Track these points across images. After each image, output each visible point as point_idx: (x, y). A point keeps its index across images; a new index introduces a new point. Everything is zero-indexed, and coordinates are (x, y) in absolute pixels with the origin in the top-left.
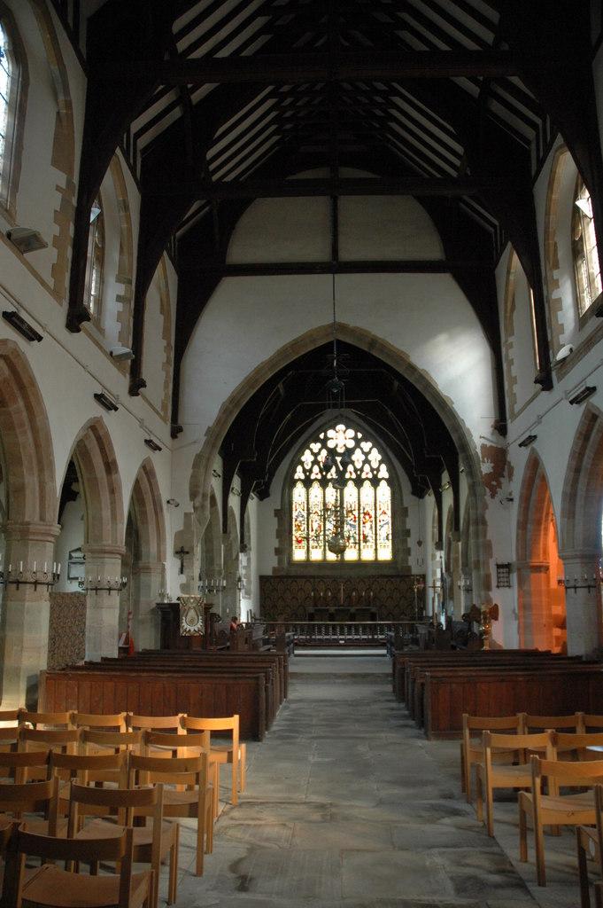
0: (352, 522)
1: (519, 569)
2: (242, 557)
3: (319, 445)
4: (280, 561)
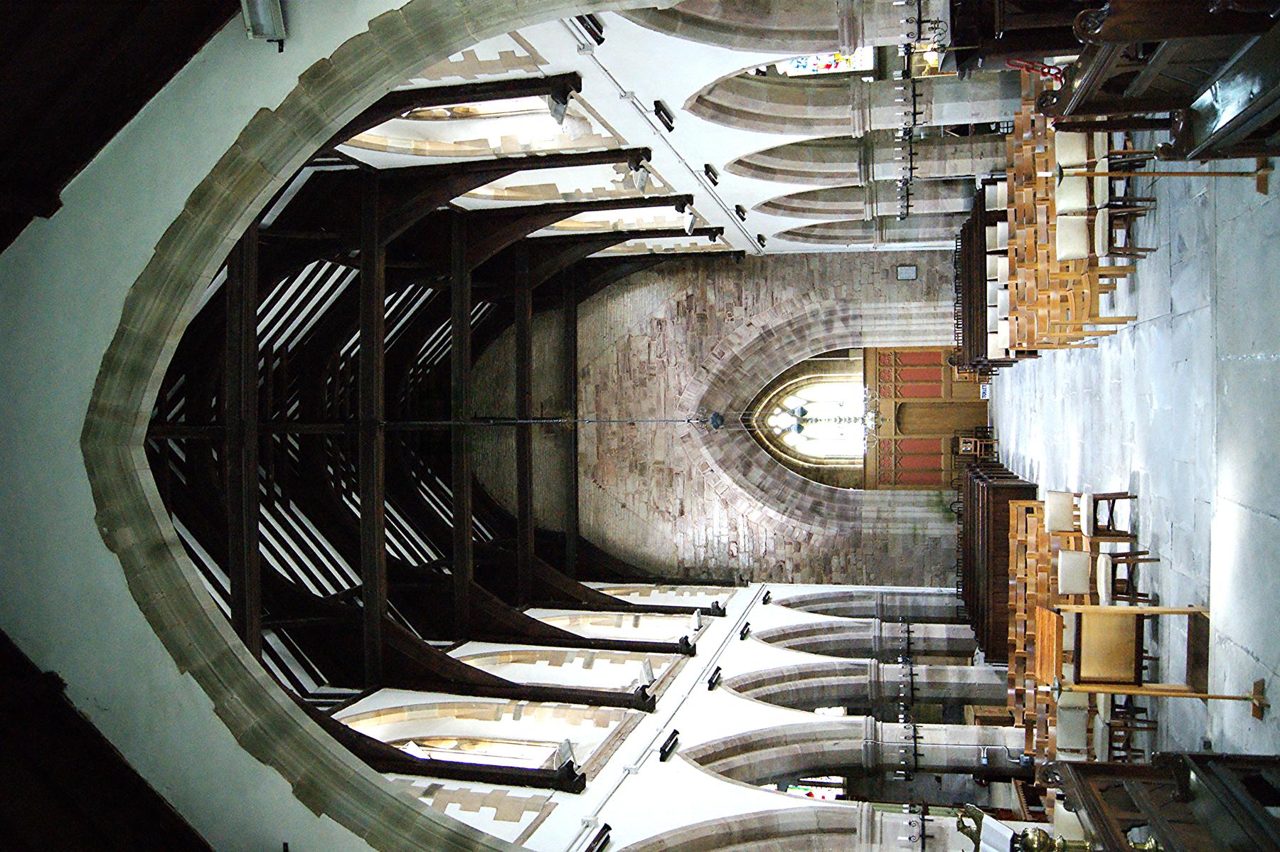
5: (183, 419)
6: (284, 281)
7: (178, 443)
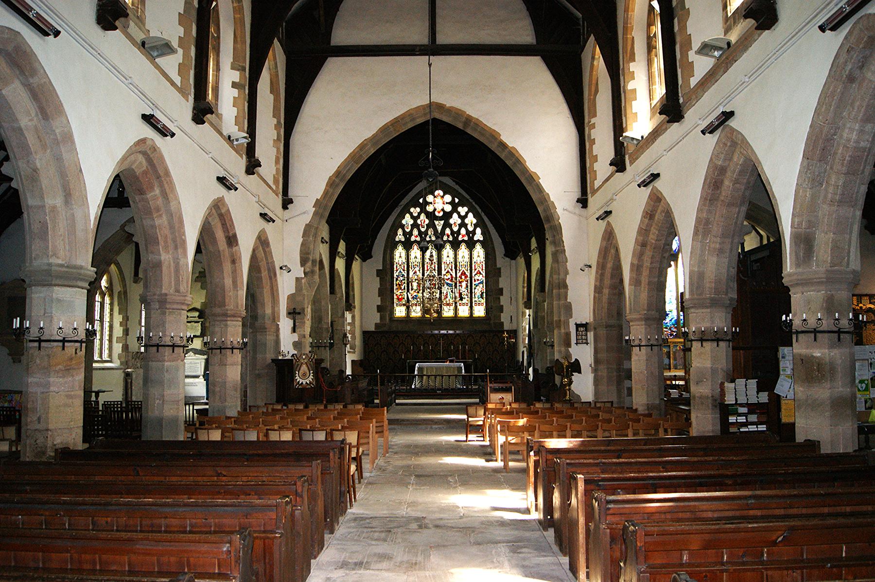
0: (449, 282)
1: (595, 329)
2: (348, 316)
3: (418, 210)
4: (381, 318)
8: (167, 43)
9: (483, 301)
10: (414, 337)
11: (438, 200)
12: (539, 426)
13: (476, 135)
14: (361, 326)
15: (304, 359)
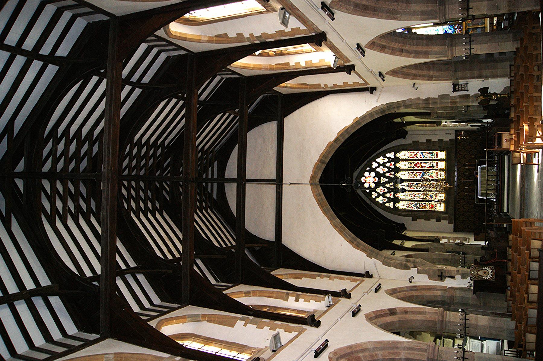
1: (457, 79)
2: (443, 241)
3: (373, 193)
4: (445, 219)
5: (169, 175)
6: (208, 122)
7: (167, 184)
8: (274, 337)
9: (435, 152)
10: (459, 198)
11: (367, 180)
12: (530, 115)
13: (330, 157)
14: (450, 233)
15: (474, 273)
